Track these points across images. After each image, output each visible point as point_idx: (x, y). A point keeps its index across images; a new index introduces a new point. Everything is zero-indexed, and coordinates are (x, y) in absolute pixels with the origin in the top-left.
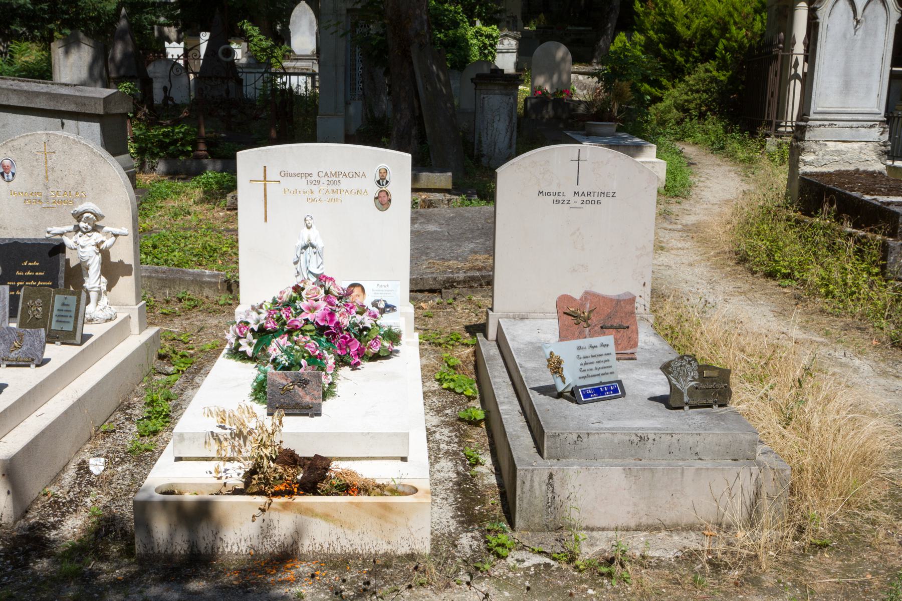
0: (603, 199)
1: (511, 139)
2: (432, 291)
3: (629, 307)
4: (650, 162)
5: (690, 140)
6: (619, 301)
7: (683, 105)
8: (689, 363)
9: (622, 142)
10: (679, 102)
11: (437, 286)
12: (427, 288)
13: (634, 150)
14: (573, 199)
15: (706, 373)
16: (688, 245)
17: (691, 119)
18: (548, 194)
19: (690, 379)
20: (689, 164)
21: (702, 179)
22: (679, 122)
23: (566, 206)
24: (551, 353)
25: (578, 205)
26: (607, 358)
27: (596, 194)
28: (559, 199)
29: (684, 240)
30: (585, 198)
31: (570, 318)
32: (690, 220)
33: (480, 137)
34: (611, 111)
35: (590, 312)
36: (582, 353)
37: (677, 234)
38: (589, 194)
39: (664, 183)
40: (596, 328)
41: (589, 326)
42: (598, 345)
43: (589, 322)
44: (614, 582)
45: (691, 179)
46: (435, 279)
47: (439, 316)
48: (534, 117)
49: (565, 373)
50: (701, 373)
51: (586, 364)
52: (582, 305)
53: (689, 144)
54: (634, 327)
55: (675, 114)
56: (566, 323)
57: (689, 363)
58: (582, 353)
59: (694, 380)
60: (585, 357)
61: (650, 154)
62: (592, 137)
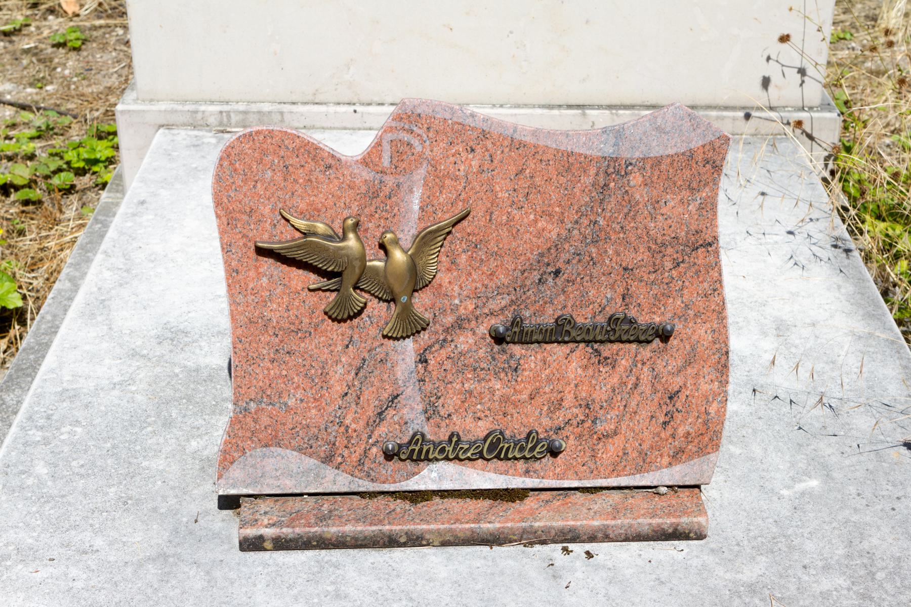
3: (676, 211)
6: (614, 170)
35: (426, 240)
40: (464, 341)
41: (410, 326)
43: (421, 302)
47: (104, 47)
54: (703, 333)
56: (274, 312)
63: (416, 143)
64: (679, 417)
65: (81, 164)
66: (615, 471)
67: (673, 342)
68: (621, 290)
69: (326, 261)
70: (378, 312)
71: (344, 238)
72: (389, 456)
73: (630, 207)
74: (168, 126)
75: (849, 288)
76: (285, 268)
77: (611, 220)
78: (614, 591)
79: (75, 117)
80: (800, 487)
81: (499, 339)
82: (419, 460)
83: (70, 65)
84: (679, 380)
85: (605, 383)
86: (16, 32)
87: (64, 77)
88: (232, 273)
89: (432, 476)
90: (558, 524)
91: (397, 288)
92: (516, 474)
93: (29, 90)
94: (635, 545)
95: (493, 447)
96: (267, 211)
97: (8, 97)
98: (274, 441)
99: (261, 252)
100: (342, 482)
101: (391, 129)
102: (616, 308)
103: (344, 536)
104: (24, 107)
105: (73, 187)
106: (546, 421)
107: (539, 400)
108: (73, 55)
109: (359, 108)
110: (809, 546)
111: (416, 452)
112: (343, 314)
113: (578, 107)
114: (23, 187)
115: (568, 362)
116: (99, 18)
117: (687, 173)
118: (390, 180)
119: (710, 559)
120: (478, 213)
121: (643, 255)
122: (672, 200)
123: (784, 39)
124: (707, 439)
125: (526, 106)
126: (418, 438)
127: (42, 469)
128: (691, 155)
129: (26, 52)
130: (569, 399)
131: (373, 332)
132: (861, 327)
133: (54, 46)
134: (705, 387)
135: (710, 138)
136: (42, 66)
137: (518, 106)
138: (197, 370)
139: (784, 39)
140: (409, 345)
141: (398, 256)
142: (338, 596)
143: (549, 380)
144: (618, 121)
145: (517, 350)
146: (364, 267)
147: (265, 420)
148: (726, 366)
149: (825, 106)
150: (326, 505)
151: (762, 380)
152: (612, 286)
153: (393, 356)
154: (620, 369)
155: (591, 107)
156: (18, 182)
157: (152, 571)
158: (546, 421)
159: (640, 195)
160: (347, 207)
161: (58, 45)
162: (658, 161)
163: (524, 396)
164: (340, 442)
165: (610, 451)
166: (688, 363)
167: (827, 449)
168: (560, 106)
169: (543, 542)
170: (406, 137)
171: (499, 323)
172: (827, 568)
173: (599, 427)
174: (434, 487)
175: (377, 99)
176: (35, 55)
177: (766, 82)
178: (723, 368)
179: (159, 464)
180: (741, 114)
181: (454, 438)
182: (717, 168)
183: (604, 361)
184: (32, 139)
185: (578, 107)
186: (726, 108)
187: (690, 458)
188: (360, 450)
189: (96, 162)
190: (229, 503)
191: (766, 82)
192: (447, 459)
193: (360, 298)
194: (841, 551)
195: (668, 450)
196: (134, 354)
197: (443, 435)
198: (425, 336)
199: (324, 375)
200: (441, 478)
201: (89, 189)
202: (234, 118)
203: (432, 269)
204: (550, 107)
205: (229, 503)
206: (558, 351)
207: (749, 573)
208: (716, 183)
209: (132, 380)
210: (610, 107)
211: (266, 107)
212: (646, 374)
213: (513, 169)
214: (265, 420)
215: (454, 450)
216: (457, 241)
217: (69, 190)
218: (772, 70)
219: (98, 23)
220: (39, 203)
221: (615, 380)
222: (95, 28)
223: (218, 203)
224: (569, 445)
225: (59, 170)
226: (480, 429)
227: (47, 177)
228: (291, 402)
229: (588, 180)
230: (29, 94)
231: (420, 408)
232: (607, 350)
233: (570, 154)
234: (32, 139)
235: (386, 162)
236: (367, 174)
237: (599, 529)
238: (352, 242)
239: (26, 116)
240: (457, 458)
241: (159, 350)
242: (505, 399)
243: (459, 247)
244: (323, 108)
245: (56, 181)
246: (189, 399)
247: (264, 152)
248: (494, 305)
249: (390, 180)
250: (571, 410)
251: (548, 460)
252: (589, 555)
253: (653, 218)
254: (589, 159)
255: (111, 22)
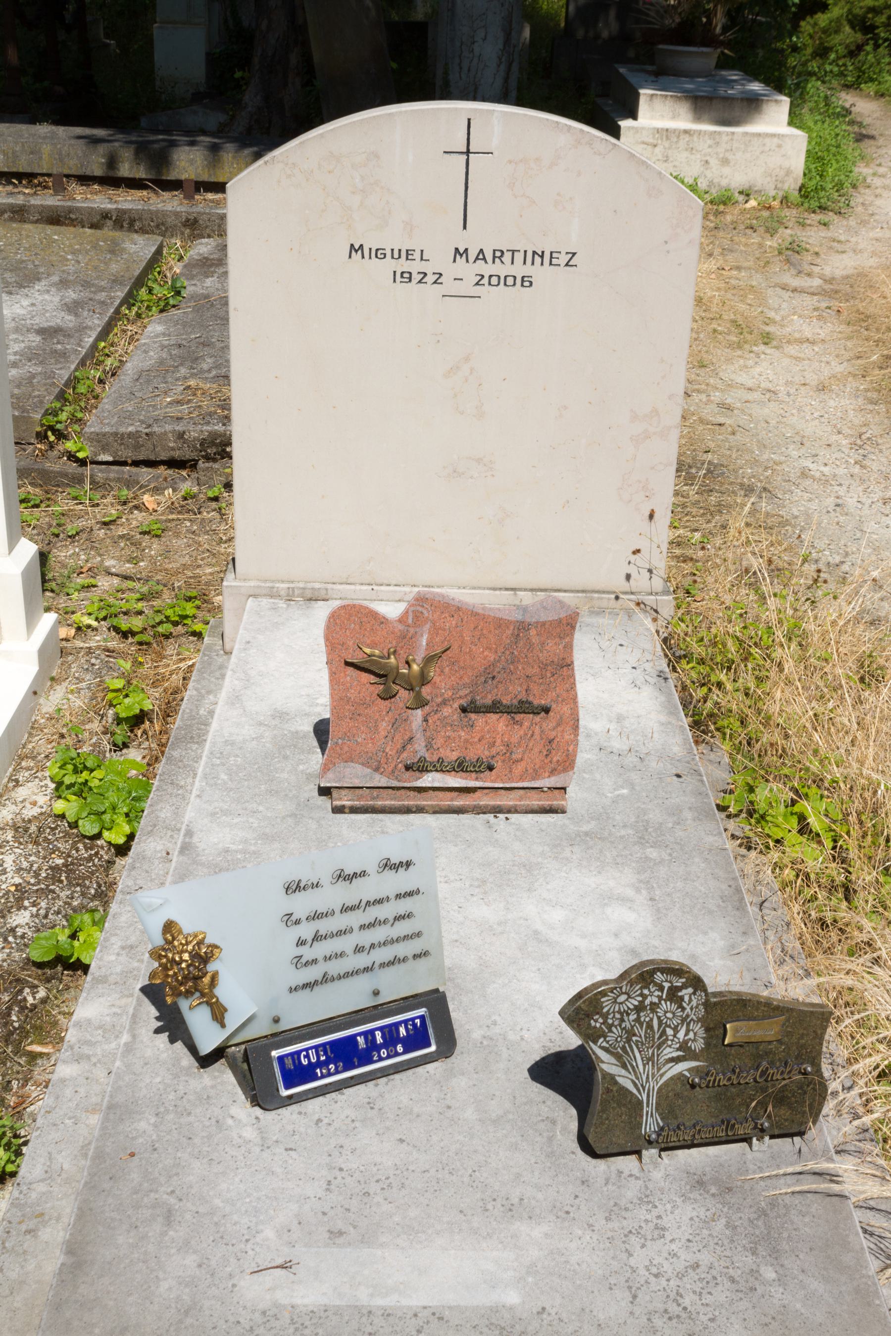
0: (539, 272)
1: (506, 79)
2: (174, 464)
3: (553, 648)
4: (773, 135)
5: (871, 88)
6: (522, 627)
7: (863, 19)
8: (673, 995)
9: (721, 91)
10: (857, 11)
11: (187, 454)
12: (164, 456)
13: (732, 110)
14: (451, 270)
15: (733, 1032)
16: (824, 330)
17: (877, 46)
18: (379, 254)
19: (669, 1052)
20: (861, 138)
21: (881, 170)
22: (854, 52)
23: (430, 291)
24: (169, 927)
25: (467, 287)
26: (403, 906)
27: (519, 257)
28: (409, 269)
29: (820, 318)
30: (487, 269)
31: (366, 677)
32: (839, 265)
33: (446, 73)
34: (710, 22)
35: (429, 660)
36: (302, 904)
37: (810, 301)
38: (498, 255)
39: (800, 181)
40: (446, 711)
41: (421, 703)
42: (372, 867)
43: (426, 691)
44: (632, 1007)
45: (862, 170)
46: (181, 435)
47: (177, 535)
48: (580, 34)
49: (224, 992)
50: (714, 1030)
51: (317, 938)
52: (406, 638)
53: (868, 96)
54: (566, 709)
55: (848, 35)
56: (352, 694)
57: (673, 995)
58: (302, 904)
59: (686, 1052)
60: (316, 916)
61: (775, 118)
62: (664, 79)
63: (425, 612)
64: (554, 752)
65: (177, 619)
66: (521, 779)
67: (551, 714)
68: (525, 687)
69: (380, 668)
70: (404, 695)
71: (389, 658)
72: (408, 768)
73: (530, 646)
74: (255, 596)
75: (663, 698)
76: (359, 672)
77: (520, 652)
78: (518, 833)
79: (165, 586)
80: (617, 793)
81: (464, 710)
82: (422, 771)
83: (154, 548)
84: (554, 733)
85: (517, 734)
86: (113, 522)
87: (151, 556)
88: (333, 674)
89: (429, 780)
90: (492, 803)
91: (414, 684)
92: (472, 779)
93: (127, 565)
94: (530, 816)
95: (460, 765)
96: (351, 644)
97: (114, 570)
98: (350, 759)
99: (347, 664)
100: (383, 781)
101: (413, 605)
102: (523, 696)
103: (385, 806)
104: (126, 578)
105: (171, 633)
106: (487, 753)
107: (484, 742)
108: (156, 540)
109: (375, 587)
110: (618, 817)
111: (421, 767)
112: (388, 696)
113: (512, 589)
114: (137, 633)
115: (498, 723)
116: (172, 513)
117: (558, 630)
118: (412, 630)
119: (567, 822)
120: (455, 647)
121: (536, 670)
122: (551, 643)
123: (637, 552)
124: (568, 764)
125: (479, 588)
126: (422, 760)
127: (224, 776)
128: (560, 621)
129: (122, 537)
130: (499, 741)
131: (401, 705)
132: (663, 718)
133: (141, 533)
134: (567, 737)
135: (570, 612)
136: (134, 548)
137: (474, 588)
138: (297, 732)
139: (637, 552)
140: (419, 712)
141: (415, 667)
142: (383, 832)
143: (489, 732)
144: (537, 599)
145: (473, 716)
146: (398, 672)
147: (346, 749)
148: (577, 727)
149: (666, 592)
150: (375, 793)
151: (605, 744)
152: (521, 685)
153: (411, 718)
154: (524, 727)
155: (520, 590)
156: (135, 629)
157: (290, 821)
158: (487, 753)
159: (535, 640)
160: (390, 642)
161: (144, 533)
162: (544, 624)
163: (476, 740)
164: (383, 760)
165: (519, 768)
166: (558, 725)
167: (634, 776)
168: (500, 589)
169: (484, 813)
170: (420, 609)
171: (464, 702)
172: (625, 826)
173: (514, 756)
174: (429, 785)
175: (386, 582)
176: (128, 539)
177: (628, 577)
178: (576, 728)
179: (285, 775)
180: (613, 596)
181: (441, 760)
182: (573, 628)
183: (516, 723)
184: (139, 600)
185: (512, 589)
186: (604, 592)
187: (559, 773)
188: (393, 765)
189: (186, 617)
190: (325, 792)
191: (628, 577)
192: (437, 771)
193: (396, 688)
194: (633, 820)
195: (548, 769)
196: (260, 724)
197: (435, 758)
198: (427, 708)
199: (376, 727)
200: (433, 780)
201: (182, 635)
202: (297, 592)
203: (432, 674)
204: (494, 589)
205: (325, 792)
206: (493, 717)
207: (585, 828)
208: (572, 635)
209: (262, 737)
210: (532, 590)
211: (317, 586)
212: (537, 730)
213: (472, 626)
214: (346, 749)
215: (440, 767)
216: (444, 661)
217: (167, 637)
218: (632, 570)
219: (171, 517)
220: (148, 644)
221: (522, 733)
222: (170, 521)
223: (327, 639)
224: (498, 764)
225: (161, 622)
226: (454, 756)
227: (153, 627)
228: (359, 740)
229: (509, 632)
230: (128, 568)
231: (423, 744)
232: (518, 717)
233: (501, 619)
234: (139, 600)
235: (410, 621)
236: (401, 627)
237: (512, 807)
238: (392, 660)
239: (130, 584)
240: (442, 771)
241: (274, 723)
242: (466, 741)
243: (445, 664)
244: (352, 587)
245: (160, 629)
246: (295, 746)
247: (350, 615)
248: (462, 693)
249: (412, 630)
250: (499, 748)
251: (487, 773)
252: (507, 819)
253: (541, 652)
254: (510, 622)
255: (180, 517)
